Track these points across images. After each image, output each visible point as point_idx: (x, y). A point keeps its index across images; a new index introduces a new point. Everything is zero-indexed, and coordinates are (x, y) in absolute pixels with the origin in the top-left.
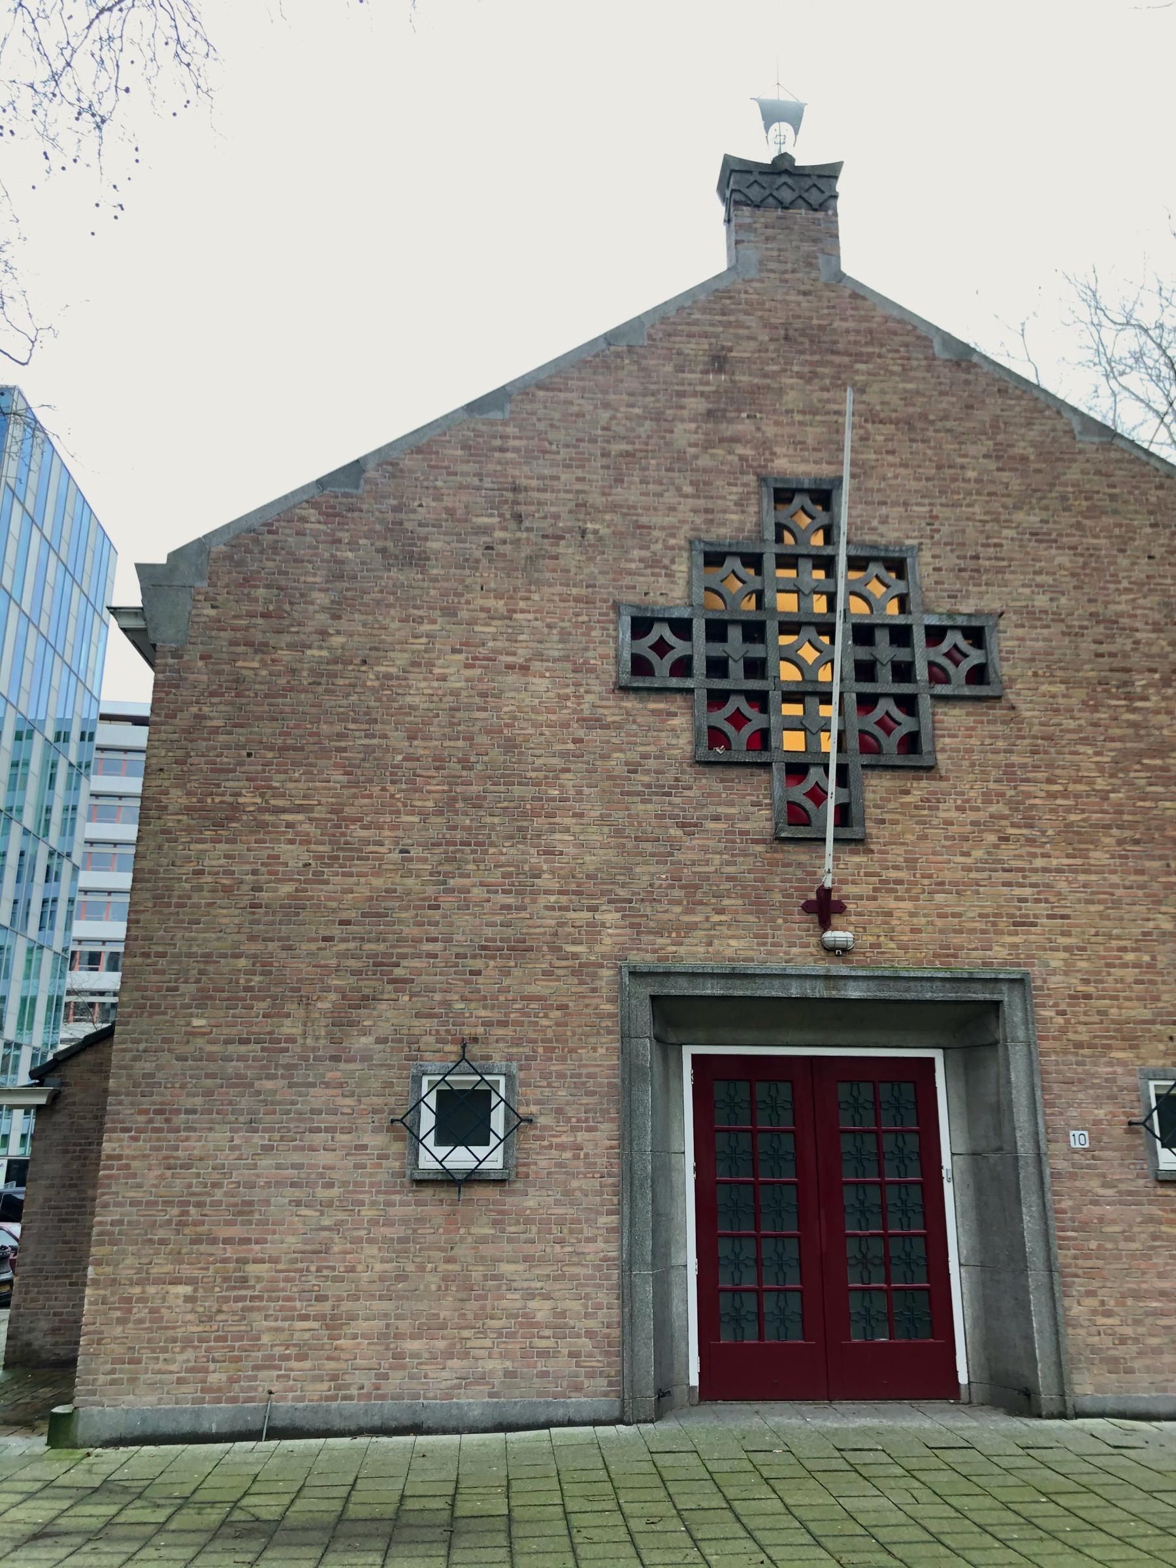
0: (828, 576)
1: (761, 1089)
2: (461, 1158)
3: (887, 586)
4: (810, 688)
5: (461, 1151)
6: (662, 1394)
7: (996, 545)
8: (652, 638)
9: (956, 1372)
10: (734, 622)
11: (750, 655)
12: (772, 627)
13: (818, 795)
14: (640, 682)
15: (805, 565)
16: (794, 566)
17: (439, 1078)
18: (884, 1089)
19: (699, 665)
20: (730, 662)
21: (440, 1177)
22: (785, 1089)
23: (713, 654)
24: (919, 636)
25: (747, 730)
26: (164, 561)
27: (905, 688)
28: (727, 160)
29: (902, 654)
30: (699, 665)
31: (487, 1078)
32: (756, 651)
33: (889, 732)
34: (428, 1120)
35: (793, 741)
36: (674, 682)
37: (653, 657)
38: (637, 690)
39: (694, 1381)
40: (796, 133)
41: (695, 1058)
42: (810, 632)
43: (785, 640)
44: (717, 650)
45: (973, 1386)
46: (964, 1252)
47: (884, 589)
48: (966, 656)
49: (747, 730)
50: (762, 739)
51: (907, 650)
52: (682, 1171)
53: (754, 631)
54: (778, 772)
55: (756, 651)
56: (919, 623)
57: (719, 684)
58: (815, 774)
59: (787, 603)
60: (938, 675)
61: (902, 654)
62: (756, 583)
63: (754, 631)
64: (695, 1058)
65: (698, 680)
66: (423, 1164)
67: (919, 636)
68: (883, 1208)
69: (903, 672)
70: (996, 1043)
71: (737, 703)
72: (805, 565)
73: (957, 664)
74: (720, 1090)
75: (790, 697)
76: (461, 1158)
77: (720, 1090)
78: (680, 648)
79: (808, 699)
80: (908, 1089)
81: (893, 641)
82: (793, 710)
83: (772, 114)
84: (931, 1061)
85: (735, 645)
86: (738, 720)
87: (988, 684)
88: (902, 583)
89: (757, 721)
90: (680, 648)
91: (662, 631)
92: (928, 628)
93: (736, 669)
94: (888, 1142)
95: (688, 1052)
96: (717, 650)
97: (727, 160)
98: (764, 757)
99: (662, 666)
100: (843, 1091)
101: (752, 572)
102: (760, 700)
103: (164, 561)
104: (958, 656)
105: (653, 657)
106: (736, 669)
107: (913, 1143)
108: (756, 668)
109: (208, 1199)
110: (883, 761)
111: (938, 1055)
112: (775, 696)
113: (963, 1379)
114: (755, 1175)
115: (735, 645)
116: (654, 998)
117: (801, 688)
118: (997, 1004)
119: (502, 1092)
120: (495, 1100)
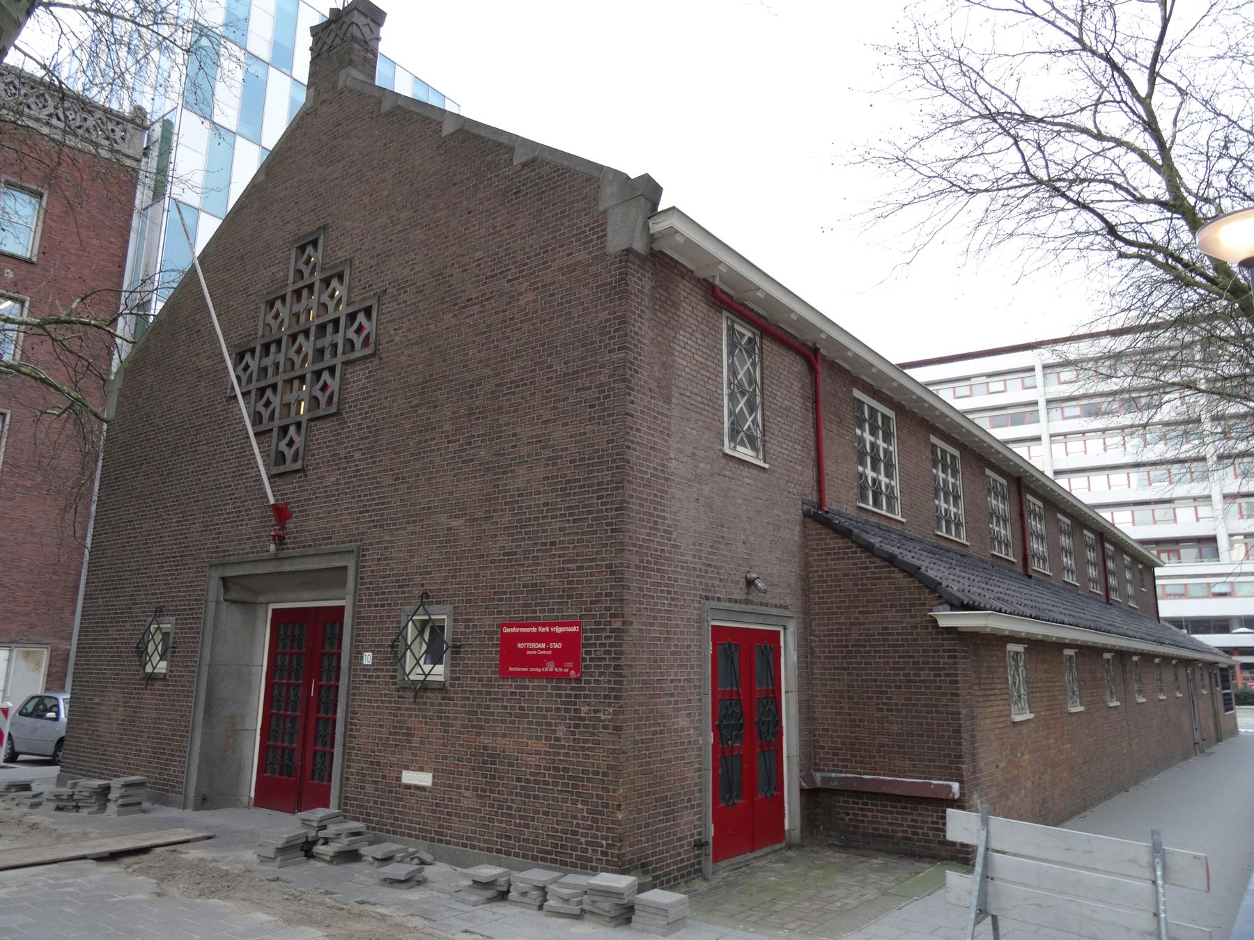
39: (253, 795)
116: (224, 580)
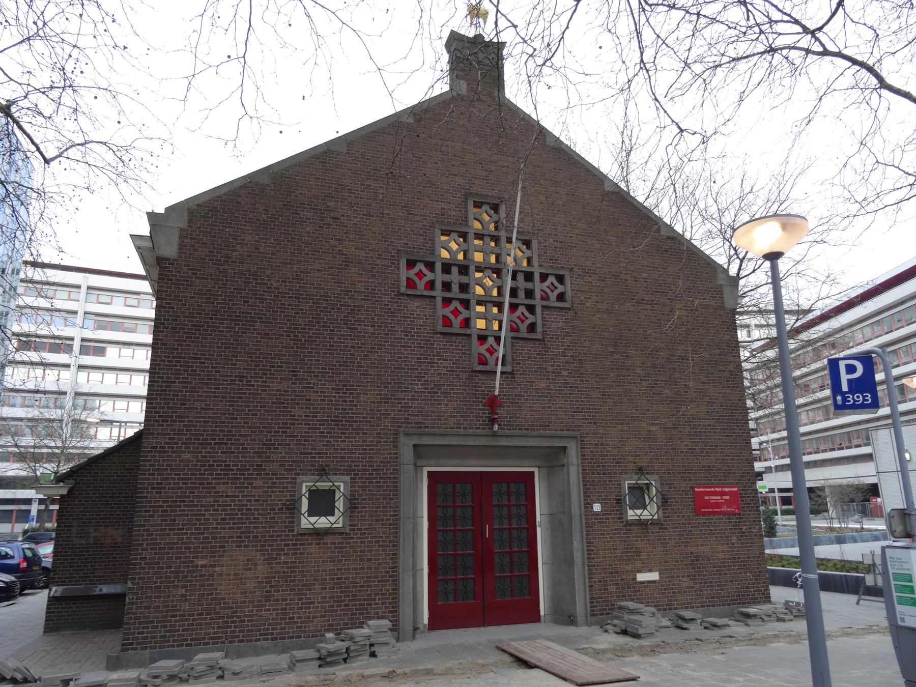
0: (496, 245)
1: (458, 487)
2: (323, 522)
3: (523, 253)
4: (489, 299)
5: (323, 519)
6: (416, 629)
7: (570, 237)
8: (416, 270)
9: (539, 611)
10: (455, 265)
11: (462, 281)
12: (472, 268)
13: (491, 351)
14: (410, 292)
15: (487, 239)
16: (482, 239)
17: (312, 484)
18: (512, 486)
19: (438, 285)
20: (453, 284)
21: (311, 532)
22: (469, 487)
23: (445, 280)
24: (537, 277)
25: (460, 318)
26: (163, 212)
27: (464, 296)
28: (452, 31)
29: (529, 285)
30: (438, 285)
31: (336, 484)
32: (464, 279)
33: (523, 321)
34: (305, 506)
35: (481, 324)
36: (427, 293)
37: (416, 279)
38: (408, 295)
39: (426, 621)
40: (485, 23)
41: (429, 473)
42: (488, 272)
43: (478, 275)
44: (447, 278)
45: (547, 616)
46: (545, 558)
47: (522, 254)
48: (548, 287)
49: (460, 318)
50: (466, 323)
51: (466, 278)
52: (422, 526)
53: (464, 270)
54: (474, 339)
55: (464, 279)
56: (537, 271)
57: (448, 295)
58: (491, 340)
59: (478, 257)
60: (545, 297)
61: (529, 285)
62: (465, 246)
63: (464, 270)
64: (429, 473)
65: (438, 292)
66: (303, 526)
67: (537, 277)
68: (510, 539)
69: (529, 294)
70: (563, 465)
71: (455, 304)
72: (487, 239)
73: (552, 291)
74: (440, 487)
75: (479, 303)
76: (323, 522)
77: (440, 487)
78: (429, 276)
79: (487, 304)
80: (522, 487)
81: (460, 273)
82: (480, 309)
83: (476, 12)
84: (533, 473)
85: (455, 277)
86: (456, 313)
87: (566, 301)
88: (466, 245)
89: (465, 314)
90: (429, 276)
91: (420, 266)
92: (541, 274)
93: (455, 288)
94: (514, 510)
95: (627, 482)
96: (447, 278)
97: (452, 31)
98: (468, 331)
99: (421, 284)
100: (495, 487)
101: (461, 240)
102: (466, 304)
103: (163, 212)
104: (552, 288)
105: (416, 279)
106: (455, 288)
107: (523, 511)
108: (464, 288)
109: (209, 545)
110: (520, 335)
111: (536, 470)
112: (473, 302)
113: (542, 613)
114: (455, 527)
115: (455, 277)
117: (484, 299)
118: (565, 448)
119: (342, 490)
120: (337, 495)
